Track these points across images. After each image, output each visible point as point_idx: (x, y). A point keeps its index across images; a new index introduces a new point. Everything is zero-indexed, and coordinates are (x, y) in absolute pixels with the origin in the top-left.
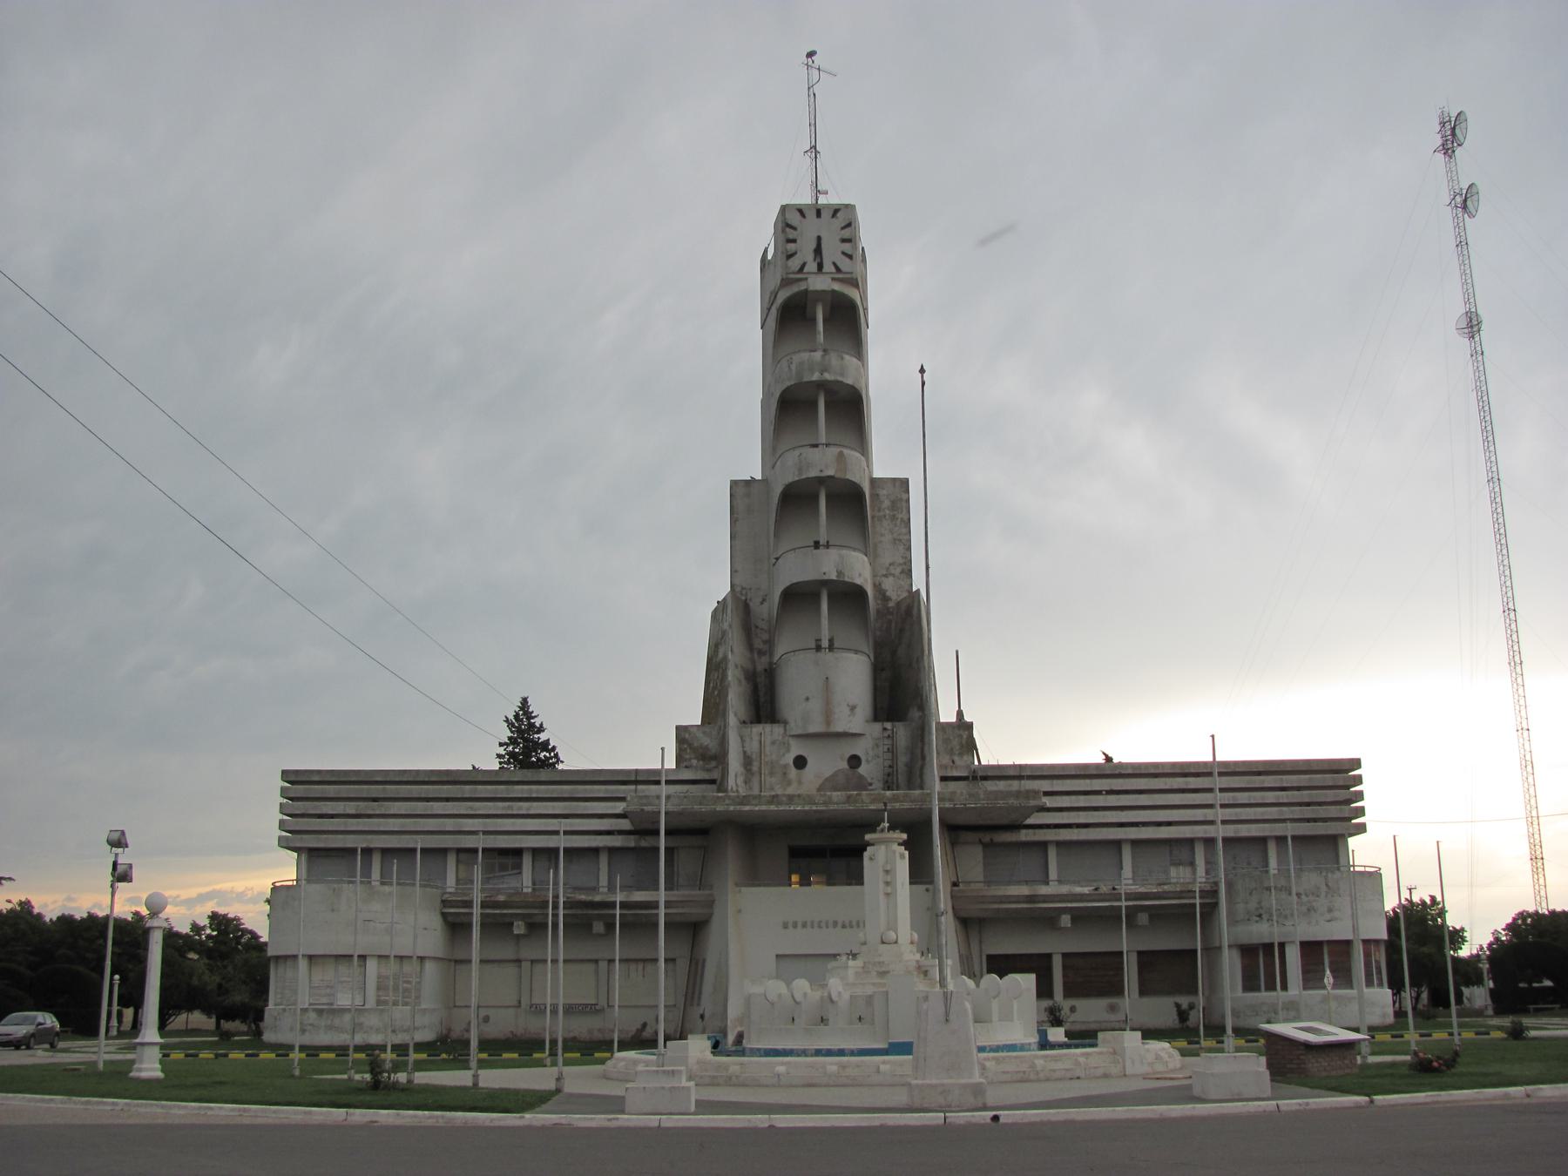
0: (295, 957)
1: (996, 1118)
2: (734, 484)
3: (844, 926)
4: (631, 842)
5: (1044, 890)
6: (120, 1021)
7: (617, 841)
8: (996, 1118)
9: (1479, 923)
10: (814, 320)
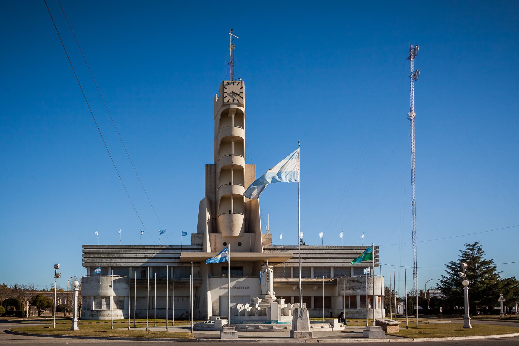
1: (318, 341)
4: (179, 265)
5: (290, 280)
6: (49, 317)
7: (176, 265)
8: (318, 341)
9: (84, 272)
10: (231, 118)
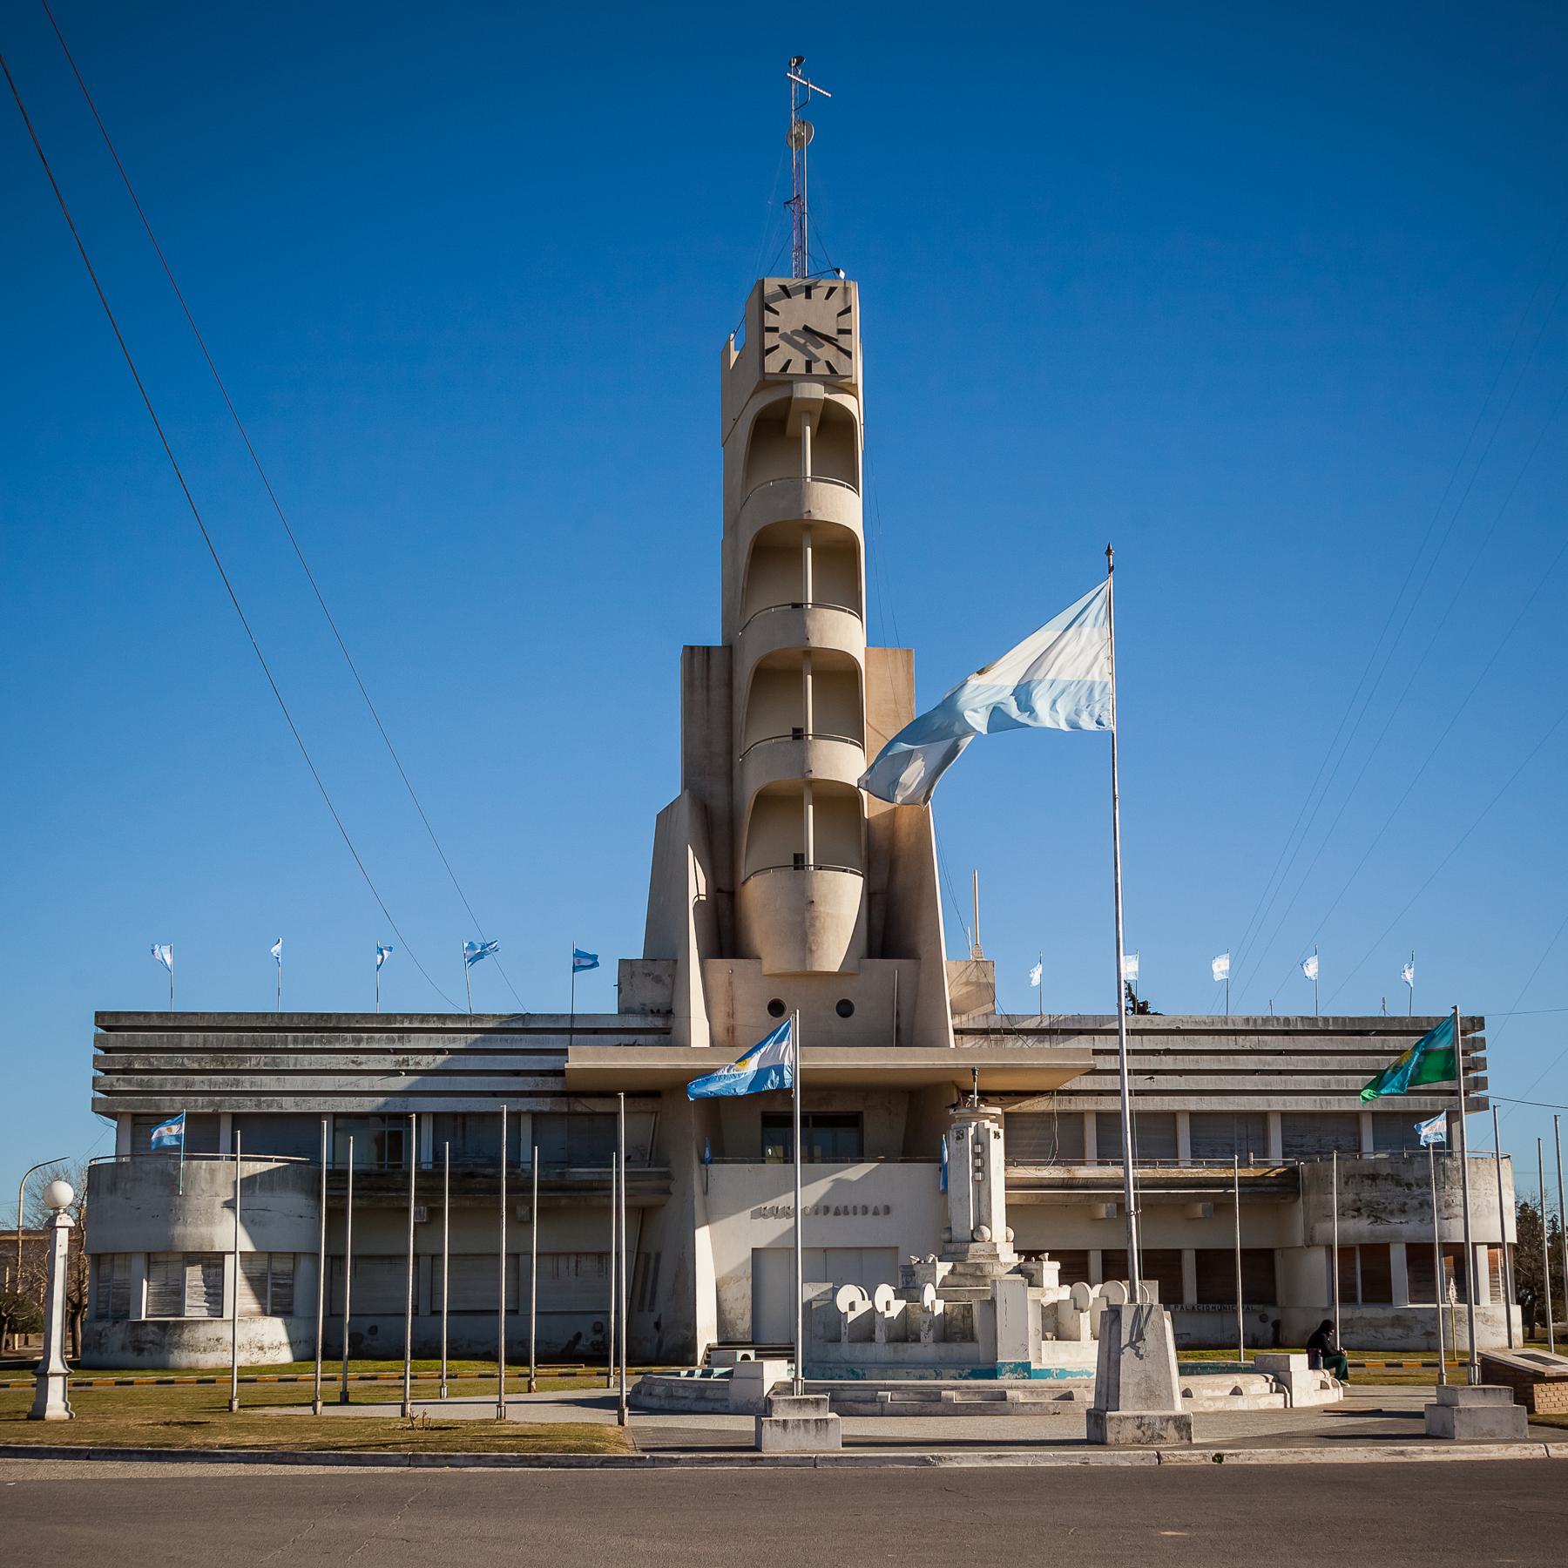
0: (127, 1255)
2: (690, 651)
3: (837, 1213)
7: (544, 1105)
10: (799, 440)
